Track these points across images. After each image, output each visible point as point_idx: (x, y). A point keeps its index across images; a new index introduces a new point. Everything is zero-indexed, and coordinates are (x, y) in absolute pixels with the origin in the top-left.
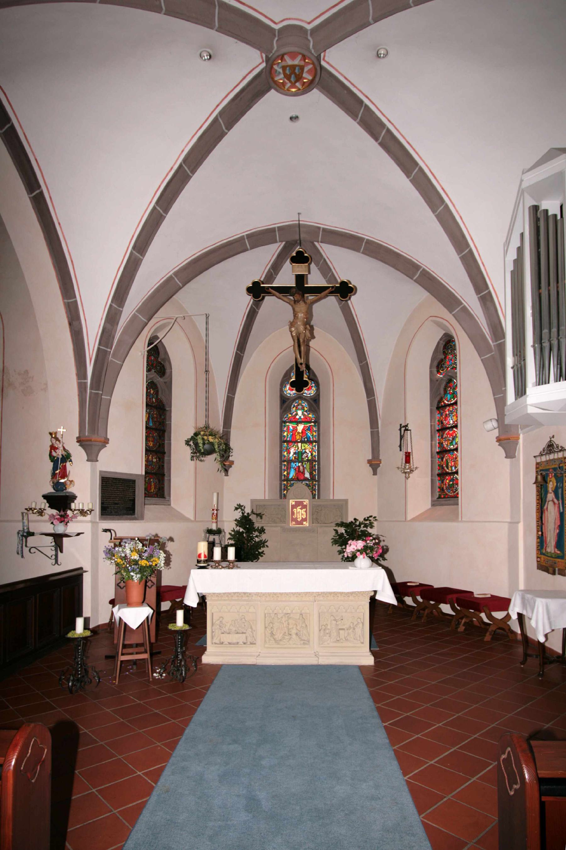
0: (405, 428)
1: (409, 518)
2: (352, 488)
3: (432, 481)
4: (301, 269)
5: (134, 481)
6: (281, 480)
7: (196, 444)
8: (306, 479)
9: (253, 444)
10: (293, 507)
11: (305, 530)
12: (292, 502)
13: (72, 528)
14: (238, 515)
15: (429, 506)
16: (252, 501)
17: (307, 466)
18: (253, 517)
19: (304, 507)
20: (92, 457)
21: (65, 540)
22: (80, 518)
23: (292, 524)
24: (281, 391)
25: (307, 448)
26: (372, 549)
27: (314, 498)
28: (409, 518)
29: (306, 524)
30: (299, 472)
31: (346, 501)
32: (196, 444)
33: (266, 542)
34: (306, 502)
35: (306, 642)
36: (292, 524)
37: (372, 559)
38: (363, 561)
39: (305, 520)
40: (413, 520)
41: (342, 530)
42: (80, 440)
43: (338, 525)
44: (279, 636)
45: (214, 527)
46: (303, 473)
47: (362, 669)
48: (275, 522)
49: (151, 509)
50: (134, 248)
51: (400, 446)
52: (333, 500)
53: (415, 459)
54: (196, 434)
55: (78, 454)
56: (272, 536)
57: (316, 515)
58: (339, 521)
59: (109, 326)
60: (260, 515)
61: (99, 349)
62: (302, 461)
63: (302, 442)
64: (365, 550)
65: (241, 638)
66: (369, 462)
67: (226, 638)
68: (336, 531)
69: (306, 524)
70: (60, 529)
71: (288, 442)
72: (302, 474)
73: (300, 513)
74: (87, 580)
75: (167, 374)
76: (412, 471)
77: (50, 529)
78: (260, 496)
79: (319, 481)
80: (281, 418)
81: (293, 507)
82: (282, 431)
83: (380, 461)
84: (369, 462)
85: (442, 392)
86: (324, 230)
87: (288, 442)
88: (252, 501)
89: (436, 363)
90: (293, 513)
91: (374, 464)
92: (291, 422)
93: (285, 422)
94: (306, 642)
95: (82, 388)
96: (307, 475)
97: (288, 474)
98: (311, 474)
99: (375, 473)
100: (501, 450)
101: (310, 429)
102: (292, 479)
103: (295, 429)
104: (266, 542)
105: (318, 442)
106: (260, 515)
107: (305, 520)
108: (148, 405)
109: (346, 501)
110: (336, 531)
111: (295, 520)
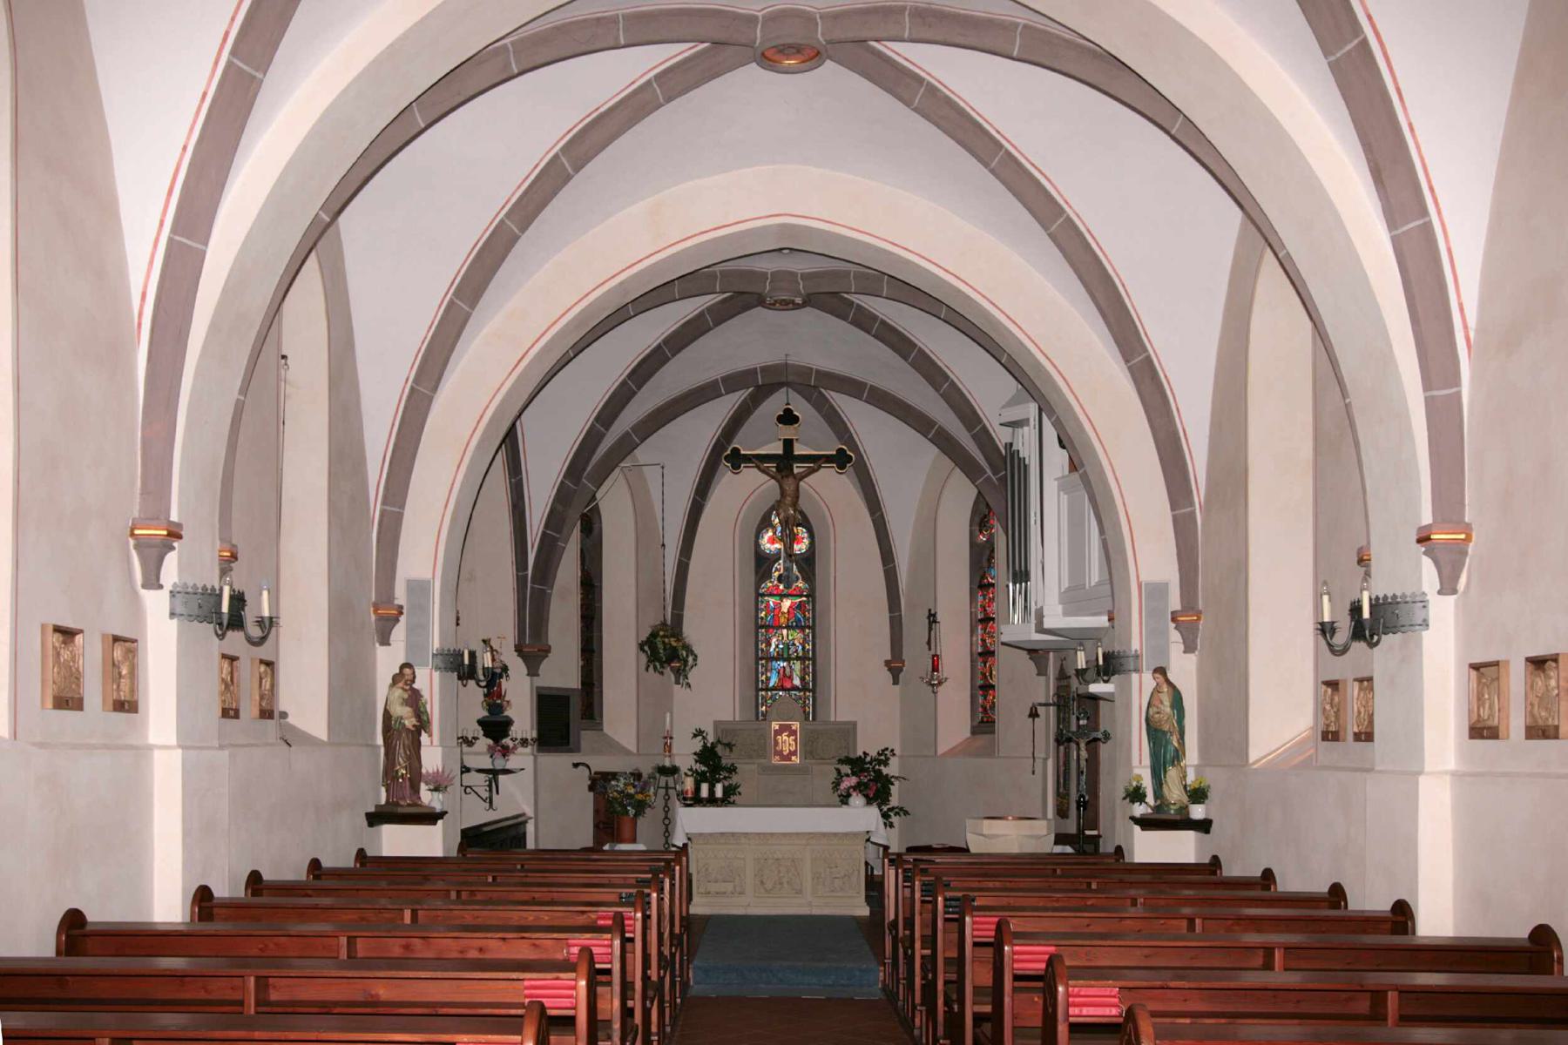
0: (932, 618)
1: (941, 749)
2: (866, 706)
3: (973, 697)
4: (787, 432)
5: (567, 698)
6: (758, 690)
7: (654, 649)
8: (795, 688)
9: (714, 628)
10: (778, 733)
11: (794, 770)
12: (775, 726)
13: (513, 762)
14: (697, 745)
15: (968, 734)
16: (717, 724)
17: (797, 666)
18: (719, 749)
19: (793, 733)
20: (533, 671)
21: (501, 778)
22: (520, 750)
23: (776, 760)
24: (757, 545)
25: (796, 636)
26: (866, 785)
27: (807, 718)
28: (940, 752)
29: (796, 760)
30: (785, 676)
31: (854, 724)
32: (654, 649)
33: (737, 786)
34: (796, 725)
35: (799, 892)
36: (776, 760)
37: (866, 796)
38: (857, 800)
39: (794, 753)
40: (944, 755)
41: (486, 660)
42: (519, 649)
43: (841, 761)
44: (769, 885)
45: (667, 763)
46: (791, 678)
47: (857, 920)
48: (750, 757)
49: (587, 737)
50: (597, 419)
51: (929, 643)
52: (835, 723)
53: (947, 668)
54: (654, 635)
55: (517, 666)
56: (747, 774)
57: (810, 747)
58: (843, 755)
59: (560, 508)
60: (729, 746)
61: (544, 534)
62: (788, 659)
63: (788, 627)
64: (858, 787)
65: (729, 887)
66: (887, 663)
67: (713, 887)
68: (838, 771)
69: (796, 760)
70: (500, 763)
71: (767, 627)
72: (791, 676)
73: (787, 743)
74: (530, 828)
75: (596, 532)
76: (940, 683)
77: (486, 763)
78: (727, 716)
79: (813, 691)
80: (758, 587)
81: (778, 733)
82: (757, 610)
83: (903, 662)
84: (887, 663)
85: (985, 564)
86: (818, 371)
87: (767, 627)
88: (717, 724)
89: (977, 520)
90: (776, 743)
91: (895, 668)
92: (771, 595)
93: (763, 595)
94: (799, 892)
95: (521, 582)
96: (797, 682)
97: (768, 679)
98: (802, 679)
99: (896, 682)
100: (1032, 664)
101: (801, 606)
102: (774, 689)
103: (778, 606)
104: (737, 786)
105: (813, 628)
106: (729, 746)
107: (794, 753)
108: (582, 584)
109: (854, 724)
110: (838, 771)
111: (780, 753)
